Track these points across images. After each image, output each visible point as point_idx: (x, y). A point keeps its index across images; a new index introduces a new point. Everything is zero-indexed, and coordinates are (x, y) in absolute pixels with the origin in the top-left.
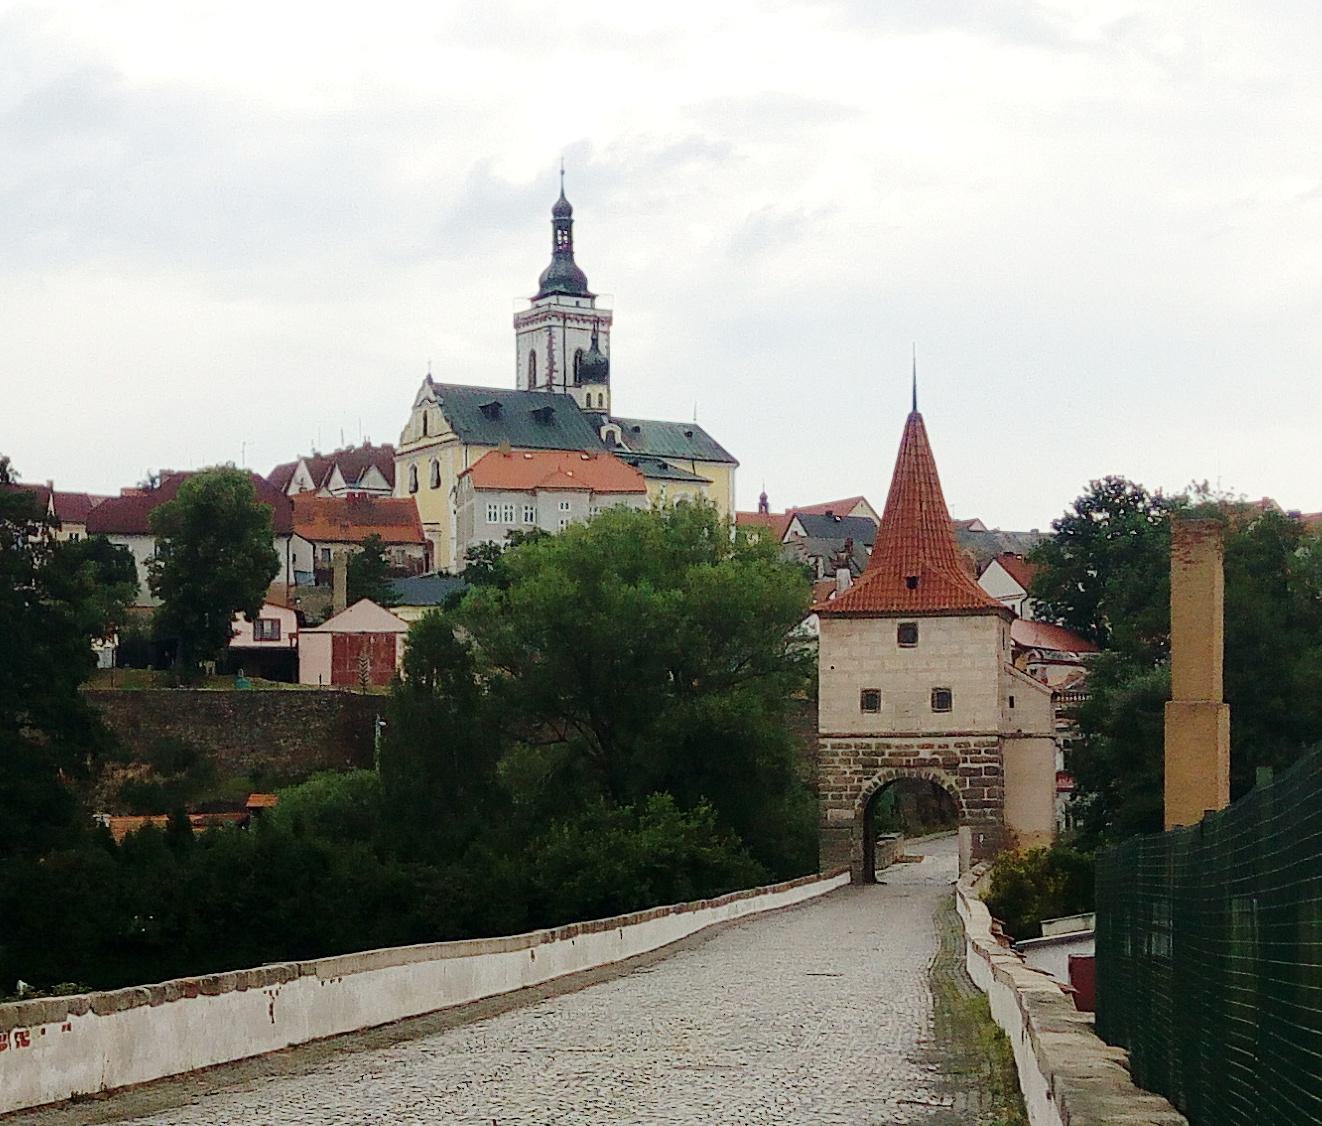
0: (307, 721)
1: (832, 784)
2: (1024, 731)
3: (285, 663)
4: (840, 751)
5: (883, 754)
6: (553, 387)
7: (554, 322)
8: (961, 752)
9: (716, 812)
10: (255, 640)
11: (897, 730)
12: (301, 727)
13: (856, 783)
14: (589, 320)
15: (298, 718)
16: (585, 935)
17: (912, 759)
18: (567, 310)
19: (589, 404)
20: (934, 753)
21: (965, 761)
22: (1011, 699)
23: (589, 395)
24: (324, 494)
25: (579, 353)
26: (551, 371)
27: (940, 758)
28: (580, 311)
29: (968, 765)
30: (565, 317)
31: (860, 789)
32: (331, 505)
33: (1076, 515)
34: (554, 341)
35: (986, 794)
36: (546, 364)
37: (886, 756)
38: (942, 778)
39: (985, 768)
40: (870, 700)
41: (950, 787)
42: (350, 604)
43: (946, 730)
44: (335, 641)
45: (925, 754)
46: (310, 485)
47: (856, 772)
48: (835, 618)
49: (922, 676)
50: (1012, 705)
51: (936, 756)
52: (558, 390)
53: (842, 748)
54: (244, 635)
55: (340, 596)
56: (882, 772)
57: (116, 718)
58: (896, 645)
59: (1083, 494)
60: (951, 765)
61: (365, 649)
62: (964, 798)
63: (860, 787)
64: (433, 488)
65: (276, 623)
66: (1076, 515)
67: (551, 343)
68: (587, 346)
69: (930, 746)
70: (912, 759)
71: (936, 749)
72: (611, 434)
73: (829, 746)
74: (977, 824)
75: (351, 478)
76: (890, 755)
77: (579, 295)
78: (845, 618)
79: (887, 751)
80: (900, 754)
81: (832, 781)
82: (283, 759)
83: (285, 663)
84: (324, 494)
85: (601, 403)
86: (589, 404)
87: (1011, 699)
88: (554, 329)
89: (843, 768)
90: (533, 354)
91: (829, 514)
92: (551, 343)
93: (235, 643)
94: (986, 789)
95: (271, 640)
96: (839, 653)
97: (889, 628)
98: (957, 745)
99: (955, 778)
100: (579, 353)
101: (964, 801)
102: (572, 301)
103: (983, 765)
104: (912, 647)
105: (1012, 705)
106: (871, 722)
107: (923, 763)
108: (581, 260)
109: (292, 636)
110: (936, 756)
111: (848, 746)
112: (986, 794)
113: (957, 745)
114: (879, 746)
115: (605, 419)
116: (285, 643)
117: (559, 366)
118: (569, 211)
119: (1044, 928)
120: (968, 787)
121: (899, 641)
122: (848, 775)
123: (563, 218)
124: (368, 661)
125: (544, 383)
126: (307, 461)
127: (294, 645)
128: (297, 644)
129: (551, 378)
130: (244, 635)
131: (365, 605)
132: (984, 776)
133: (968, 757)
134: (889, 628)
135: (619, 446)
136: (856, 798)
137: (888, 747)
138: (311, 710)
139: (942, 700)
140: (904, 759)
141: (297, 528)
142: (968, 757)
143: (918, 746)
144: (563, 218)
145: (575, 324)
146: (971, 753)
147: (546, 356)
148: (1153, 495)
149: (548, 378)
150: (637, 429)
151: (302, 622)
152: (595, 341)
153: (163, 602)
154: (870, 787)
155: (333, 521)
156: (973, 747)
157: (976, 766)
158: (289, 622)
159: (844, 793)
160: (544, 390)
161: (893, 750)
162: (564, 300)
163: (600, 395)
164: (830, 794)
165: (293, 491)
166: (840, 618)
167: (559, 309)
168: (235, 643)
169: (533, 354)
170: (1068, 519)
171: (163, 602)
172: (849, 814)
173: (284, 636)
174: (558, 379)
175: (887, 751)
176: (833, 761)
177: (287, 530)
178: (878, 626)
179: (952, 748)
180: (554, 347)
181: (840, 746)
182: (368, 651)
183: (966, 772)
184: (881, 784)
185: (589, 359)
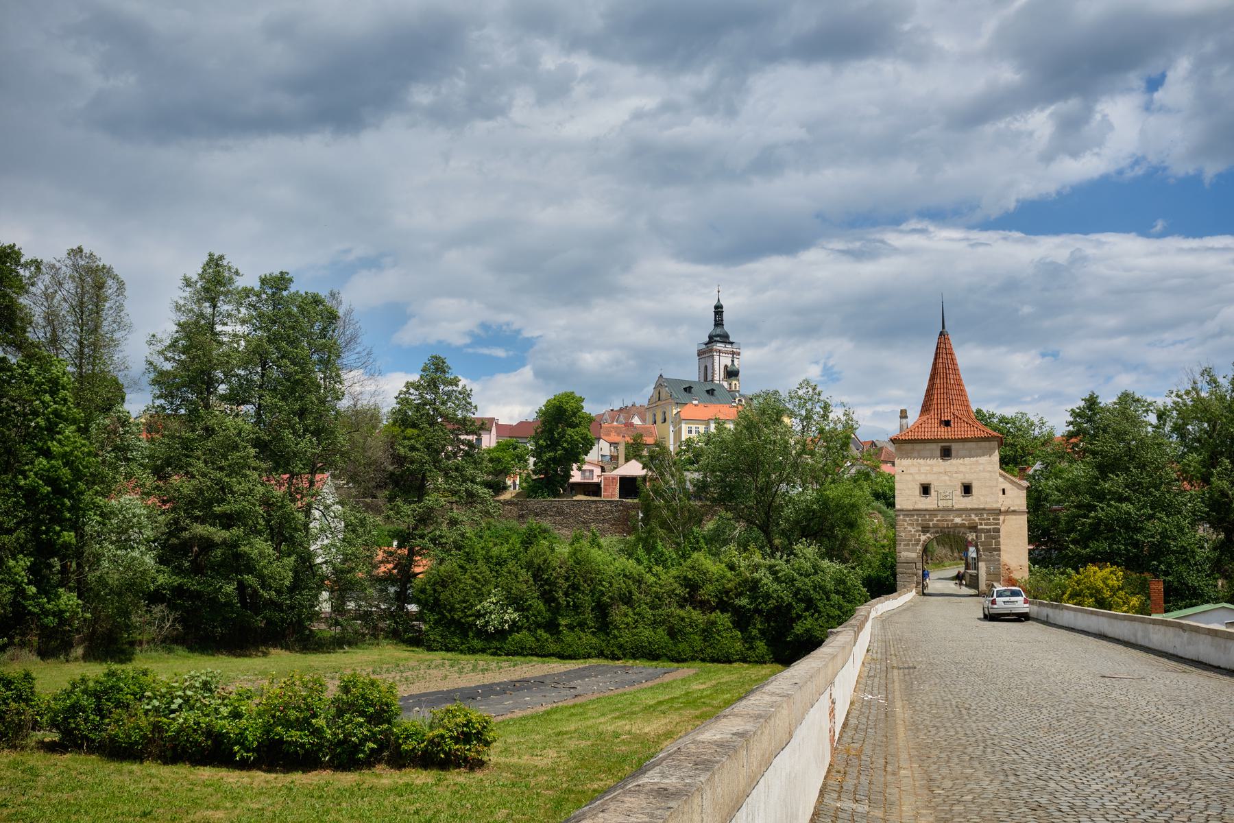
2: (1012, 508)
3: (594, 489)
5: (933, 520)
8: (979, 519)
9: (409, 586)
21: (981, 524)
22: (1004, 490)
25: (726, 366)
27: (966, 523)
29: (983, 527)
30: (720, 352)
31: (919, 540)
37: (935, 519)
40: (926, 490)
47: (917, 531)
50: (1004, 493)
54: (576, 477)
55: (622, 459)
65: (591, 471)
68: (729, 364)
74: (988, 561)
76: (938, 520)
80: (943, 520)
85: (736, 388)
87: (1004, 490)
89: (910, 528)
90: (706, 367)
93: (572, 480)
95: (589, 479)
100: (726, 366)
105: (1004, 493)
106: (929, 503)
108: (727, 328)
115: (737, 394)
116: (595, 480)
130: (576, 477)
139: (967, 489)
152: (733, 361)
155: (618, 435)
168: (572, 480)
169: (706, 367)
172: (914, 555)
173: (595, 477)
174: (717, 377)
176: (904, 525)
178: (928, 448)
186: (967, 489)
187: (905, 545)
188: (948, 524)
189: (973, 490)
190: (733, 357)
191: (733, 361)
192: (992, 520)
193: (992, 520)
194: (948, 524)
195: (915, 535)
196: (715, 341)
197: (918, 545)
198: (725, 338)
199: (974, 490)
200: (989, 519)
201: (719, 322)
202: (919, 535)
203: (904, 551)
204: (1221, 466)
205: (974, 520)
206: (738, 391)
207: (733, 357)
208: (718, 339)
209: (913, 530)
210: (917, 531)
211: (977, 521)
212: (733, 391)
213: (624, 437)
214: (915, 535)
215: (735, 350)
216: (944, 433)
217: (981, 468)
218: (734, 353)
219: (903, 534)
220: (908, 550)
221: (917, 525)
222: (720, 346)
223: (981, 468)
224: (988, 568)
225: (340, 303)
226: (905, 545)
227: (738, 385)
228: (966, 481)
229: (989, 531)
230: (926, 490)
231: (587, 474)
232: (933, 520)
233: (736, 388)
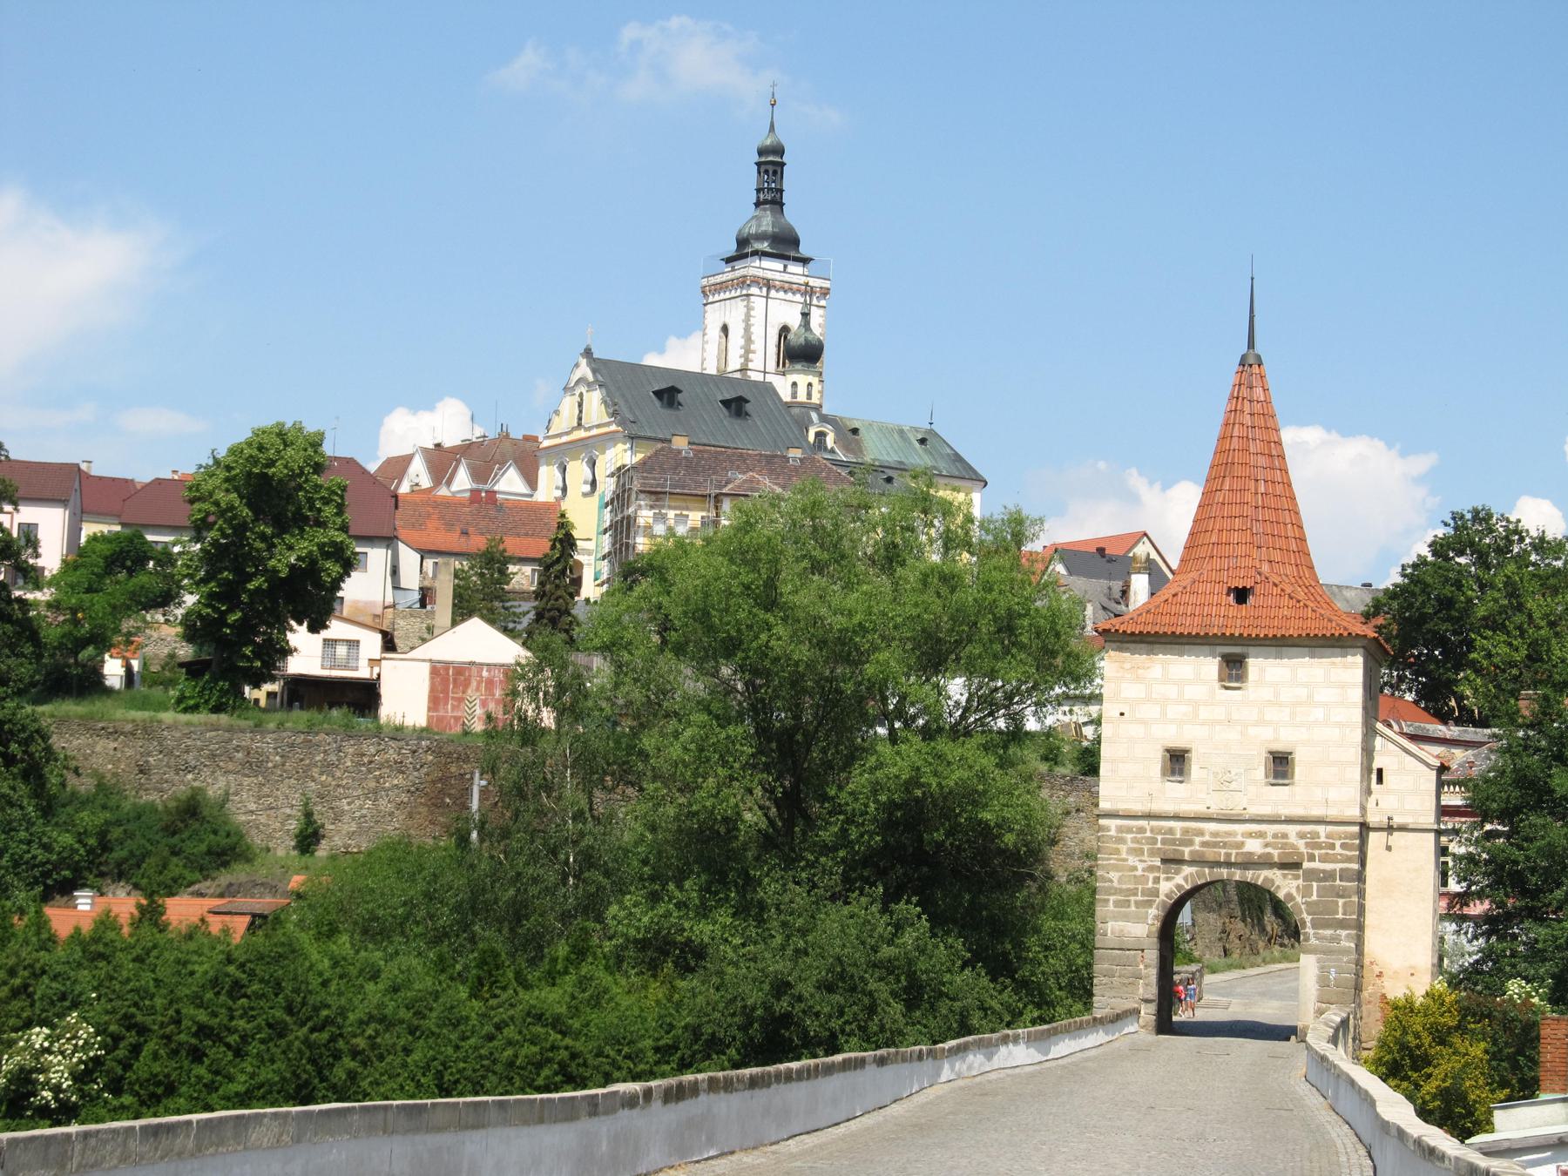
0: (381, 776)
1: (1115, 884)
4: (1129, 836)
6: (749, 373)
7: (754, 290)
8: (1307, 845)
10: (323, 667)
11: (1214, 810)
12: (373, 784)
13: (1150, 885)
14: (799, 291)
15: (370, 771)
16: (712, 1095)
17: (1234, 852)
18: (769, 275)
19: (794, 395)
20: (1267, 845)
21: (1312, 858)
23: (794, 384)
24: (443, 491)
26: (747, 351)
28: (786, 277)
29: (1316, 865)
31: (1156, 893)
32: (449, 505)
33: (1430, 558)
34: (752, 313)
35: (1340, 910)
36: (742, 342)
38: (1277, 883)
39: (1341, 870)
40: (1177, 761)
41: (1290, 896)
42: (454, 623)
43: (1285, 811)
44: (435, 672)
45: (1254, 847)
46: (426, 482)
47: (1151, 869)
48: (1128, 642)
49: (1252, 731)
51: (1269, 850)
52: (755, 376)
53: (1132, 832)
56: (1187, 870)
57: (119, 760)
58: (1217, 685)
59: (1441, 532)
60: (1290, 865)
61: (474, 684)
62: (1309, 914)
63: (1157, 891)
64: (585, 495)
66: (1430, 558)
67: (748, 317)
68: (794, 321)
69: (1261, 835)
70: (1234, 852)
71: (1269, 839)
72: (821, 435)
73: (1113, 828)
75: (480, 474)
76: (1204, 844)
77: (787, 258)
78: (1142, 642)
79: (1197, 840)
80: (1215, 845)
81: (1115, 880)
82: (346, 827)
83: (364, 696)
84: (443, 491)
85: (809, 395)
86: (794, 395)
88: (752, 298)
89: (1132, 860)
90: (725, 329)
91: (1101, 551)
92: (748, 317)
94: (1341, 902)
95: (346, 668)
96: (1132, 690)
97: (1209, 666)
98: (1301, 836)
99: (1295, 883)
100: (784, 330)
101: (1308, 918)
102: (777, 265)
103: (1338, 866)
104: (1239, 688)
106: (1174, 796)
107: (1248, 863)
108: (795, 214)
109: (373, 662)
110: (1269, 850)
111: (1141, 830)
112: (1340, 910)
113: (1301, 836)
114: (1186, 831)
115: (814, 416)
116: (363, 672)
117: (758, 345)
118: (779, 150)
119: (1499, 1117)
120: (1314, 897)
121: (1221, 680)
122: (1139, 873)
123: (771, 163)
124: (478, 701)
125: (738, 367)
126: (425, 451)
127: (375, 676)
128: (379, 675)
129: (747, 360)
131: (475, 626)
132: (1338, 882)
133: (1316, 853)
134: (1209, 666)
135: (832, 451)
136: (1151, 906)
137: (1201, 833)
138: (387, 761)
139: (1281, 764)
140: (1223, 851)
141: (401, 533)
142: (1316, 853)
143: (1243, 835)
144: (771, 163)
145: (781, 295)
146: (1321, 848)
147: (742, 332)
148: (1534, 533)
149: (742, 360)
150: (855, 431)
151: (389, 645)
152: (805, 315)
153: (83, 540)
154: (1172, 892)
155: (449, 526)
156: (1323, 839)
157: (1328, 866)
158: (371, 644)
159: (1132, 899)
160: (738, 375)
161: (1207, 838)
162: (768, 263)
163: (810, 385)
164: (1112, 898)
165: (404, 488)
166: (1134, 642)
167: (760, 273)
170: (1421, 563)
171: (83, 540)
174: (756, 363)
175: (1197, 840)
176: (1117, 851)
177: (385, 532)
179: (1293, 839)
180: (752, 321)
181: (1129, 830)
182: (478, 689)
183: (1311, 875)
184: (1188, 887)
185: (796, 338)
186: (1281, 764)
187: (1117, 904)
188: (1228, 855)
189: (1297, 770)
190: (808, 305)
191: (805, 315)
192: (1338, 850)
193: (1338, 850)
194: (1228, 855)
195: (1144, 879)
196: (755, 253)
197: (1149, 904)
198: (785, 245)
199: (1299, 771)
200: (1332, 846)
201: (771, 197)
202: (1157, 880)
203: (1115, 918)
204: (1011, 830)
205: (1293, 846)
206: (818, 408)
207: (808, 305)
208: (764, 246)
209: (1140, 866)
210: (1151, 869)
211: (1303, 849)
212: (801, 405)
213: (465, 533)
214: (1144, 879)
215: (813, 282)
216: (1236, 619)
217: (1318, 714)
218: (809, 291)
219: (1114, 875)
220: (1126, 918)
221: (1152, 853)
222: (771, 268)
223: (1318, 714)
224: (1323, 969)
225: (111, 657)
226: (1117, 904)
227: (816, 387)
228: (1279, 747)
229: (1329, 876)
230: (1177, 761)
231: (342, 651)
232: (1191, 843)
233: (809, 395)
